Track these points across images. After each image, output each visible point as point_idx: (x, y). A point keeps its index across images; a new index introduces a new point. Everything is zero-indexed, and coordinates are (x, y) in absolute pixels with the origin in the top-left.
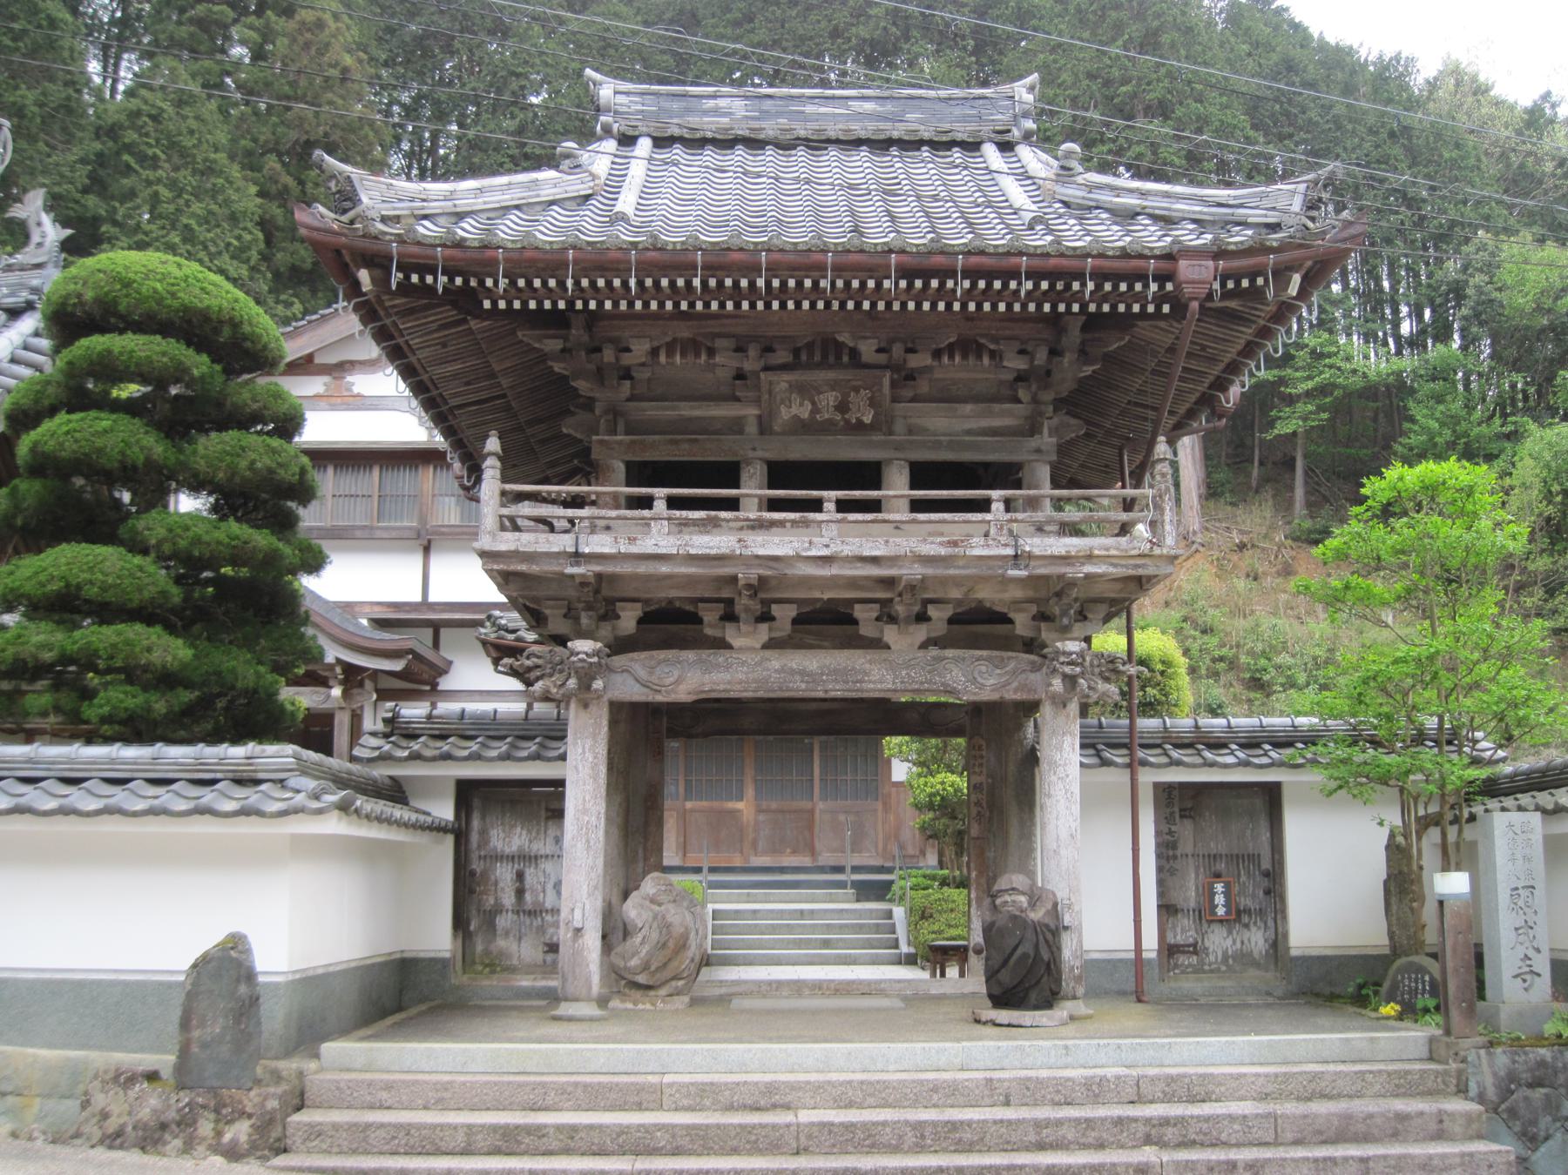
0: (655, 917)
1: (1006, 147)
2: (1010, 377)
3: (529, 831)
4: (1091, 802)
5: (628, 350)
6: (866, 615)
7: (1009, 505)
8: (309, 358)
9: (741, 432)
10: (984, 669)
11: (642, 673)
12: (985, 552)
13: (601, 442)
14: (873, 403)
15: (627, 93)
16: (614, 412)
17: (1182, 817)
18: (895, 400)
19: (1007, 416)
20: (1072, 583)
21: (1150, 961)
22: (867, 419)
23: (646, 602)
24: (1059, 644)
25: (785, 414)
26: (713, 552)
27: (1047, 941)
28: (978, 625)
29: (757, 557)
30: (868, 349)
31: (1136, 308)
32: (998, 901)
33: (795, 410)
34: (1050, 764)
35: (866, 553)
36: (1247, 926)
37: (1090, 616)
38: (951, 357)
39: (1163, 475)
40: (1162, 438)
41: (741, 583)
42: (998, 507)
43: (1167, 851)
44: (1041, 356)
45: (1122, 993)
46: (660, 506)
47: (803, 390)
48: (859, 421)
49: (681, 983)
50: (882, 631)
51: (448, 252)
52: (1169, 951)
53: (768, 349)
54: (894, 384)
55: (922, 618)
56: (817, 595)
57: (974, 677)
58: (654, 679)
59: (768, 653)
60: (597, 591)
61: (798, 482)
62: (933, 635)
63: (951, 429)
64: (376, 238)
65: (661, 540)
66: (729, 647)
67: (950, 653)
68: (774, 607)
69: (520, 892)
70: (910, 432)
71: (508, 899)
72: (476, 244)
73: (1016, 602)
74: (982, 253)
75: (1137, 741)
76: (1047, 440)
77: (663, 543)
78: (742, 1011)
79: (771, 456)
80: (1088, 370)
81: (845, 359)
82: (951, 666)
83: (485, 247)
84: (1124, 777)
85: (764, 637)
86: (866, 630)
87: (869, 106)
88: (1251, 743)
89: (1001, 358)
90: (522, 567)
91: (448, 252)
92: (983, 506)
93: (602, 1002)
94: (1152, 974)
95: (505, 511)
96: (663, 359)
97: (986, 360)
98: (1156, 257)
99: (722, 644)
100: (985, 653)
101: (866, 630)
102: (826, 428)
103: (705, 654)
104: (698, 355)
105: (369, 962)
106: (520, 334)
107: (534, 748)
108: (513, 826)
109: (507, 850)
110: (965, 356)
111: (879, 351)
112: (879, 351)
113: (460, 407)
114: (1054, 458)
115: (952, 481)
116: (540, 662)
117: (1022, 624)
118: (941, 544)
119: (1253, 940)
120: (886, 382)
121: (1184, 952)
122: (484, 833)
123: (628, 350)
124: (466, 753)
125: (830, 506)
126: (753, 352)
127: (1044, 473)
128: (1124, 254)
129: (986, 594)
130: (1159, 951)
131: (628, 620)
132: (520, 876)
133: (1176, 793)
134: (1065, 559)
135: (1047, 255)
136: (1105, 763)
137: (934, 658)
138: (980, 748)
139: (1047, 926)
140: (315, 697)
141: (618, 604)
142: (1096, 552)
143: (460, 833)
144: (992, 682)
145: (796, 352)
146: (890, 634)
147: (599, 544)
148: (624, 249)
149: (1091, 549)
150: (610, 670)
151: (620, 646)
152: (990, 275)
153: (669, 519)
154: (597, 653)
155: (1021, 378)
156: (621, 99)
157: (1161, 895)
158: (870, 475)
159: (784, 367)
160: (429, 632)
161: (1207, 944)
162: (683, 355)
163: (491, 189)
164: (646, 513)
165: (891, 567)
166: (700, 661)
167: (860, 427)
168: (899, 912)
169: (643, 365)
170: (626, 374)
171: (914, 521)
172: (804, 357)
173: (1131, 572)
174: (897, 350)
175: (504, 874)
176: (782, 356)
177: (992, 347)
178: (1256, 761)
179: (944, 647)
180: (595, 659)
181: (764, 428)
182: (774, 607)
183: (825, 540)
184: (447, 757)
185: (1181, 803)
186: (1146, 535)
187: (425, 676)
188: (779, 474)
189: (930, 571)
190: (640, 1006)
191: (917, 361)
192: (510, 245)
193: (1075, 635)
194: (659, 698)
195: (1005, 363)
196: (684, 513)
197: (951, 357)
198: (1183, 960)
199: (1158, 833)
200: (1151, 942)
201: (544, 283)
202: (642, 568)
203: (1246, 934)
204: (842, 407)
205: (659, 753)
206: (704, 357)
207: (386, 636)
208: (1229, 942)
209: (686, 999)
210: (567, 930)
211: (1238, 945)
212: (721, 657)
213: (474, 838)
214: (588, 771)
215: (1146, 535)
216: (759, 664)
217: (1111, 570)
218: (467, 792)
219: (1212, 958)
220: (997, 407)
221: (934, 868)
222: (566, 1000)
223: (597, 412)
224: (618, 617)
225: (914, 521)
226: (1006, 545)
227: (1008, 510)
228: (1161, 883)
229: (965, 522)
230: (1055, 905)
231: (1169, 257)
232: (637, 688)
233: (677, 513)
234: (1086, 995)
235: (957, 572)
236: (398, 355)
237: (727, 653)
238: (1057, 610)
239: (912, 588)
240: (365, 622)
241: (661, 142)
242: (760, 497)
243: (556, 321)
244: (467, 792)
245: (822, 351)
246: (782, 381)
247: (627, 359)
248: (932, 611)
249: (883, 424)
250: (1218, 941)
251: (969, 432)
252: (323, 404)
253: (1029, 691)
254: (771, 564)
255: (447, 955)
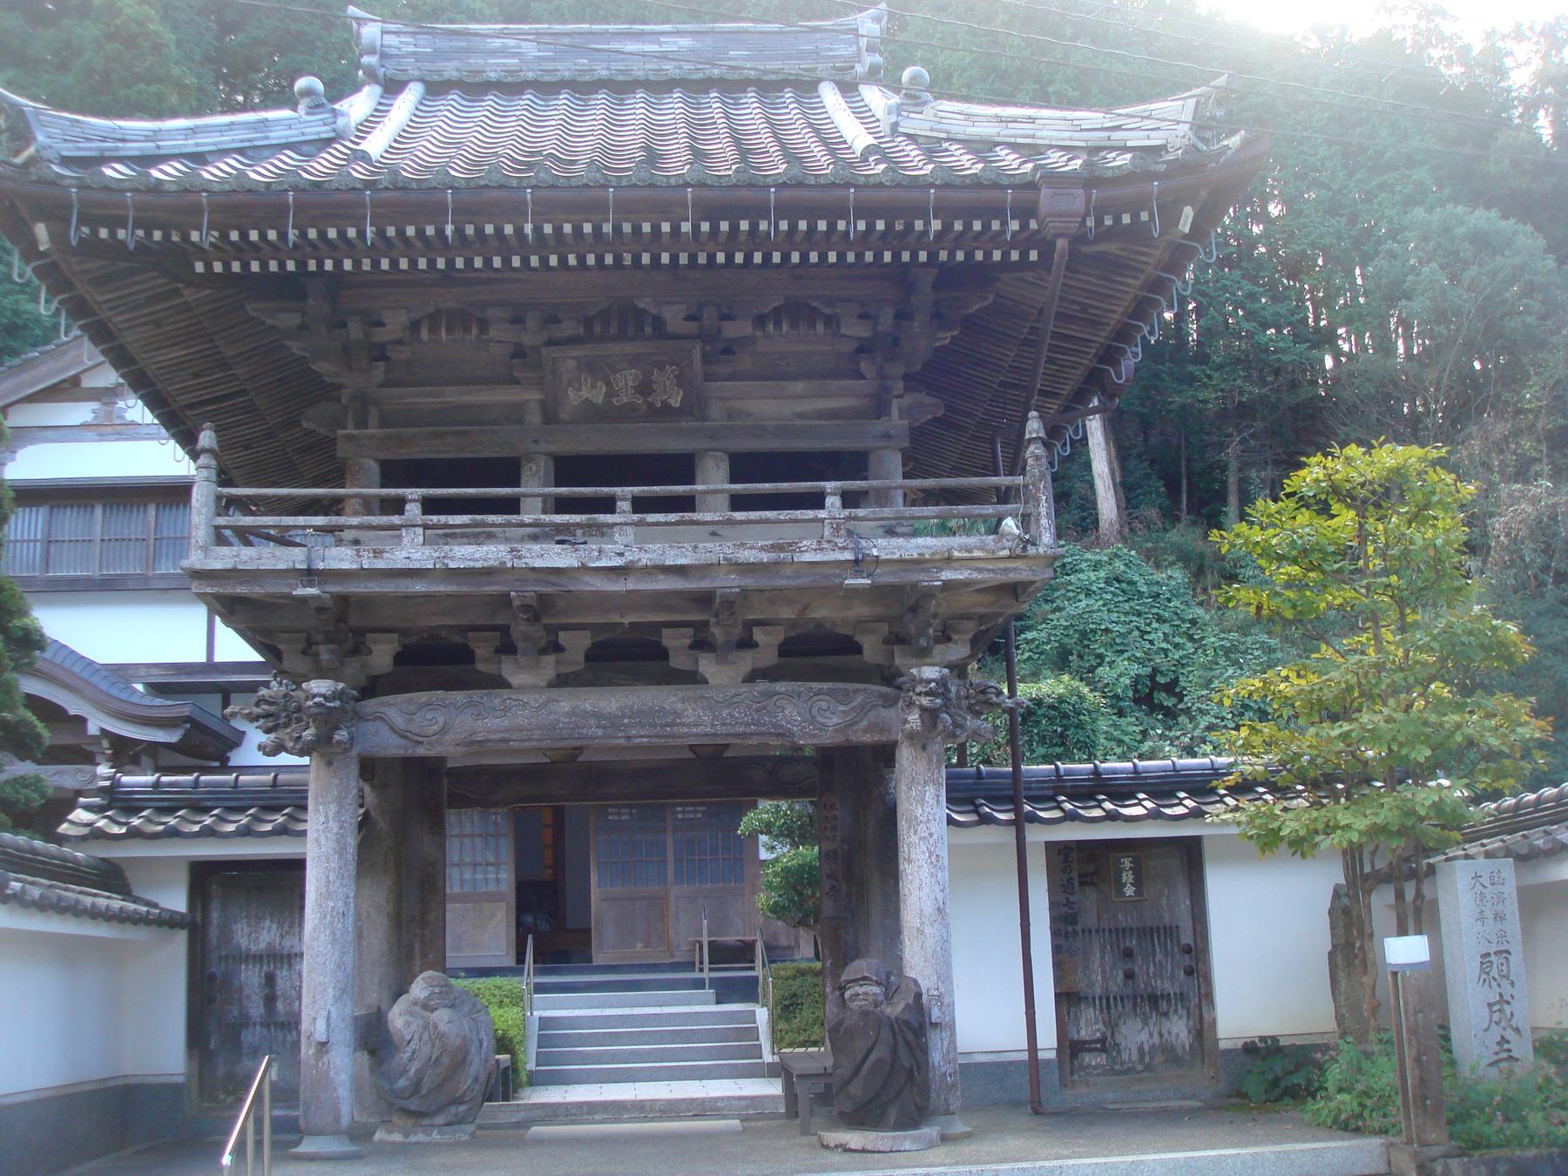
0: (426, 1027)
1: (848, 88)
2: (847, 347)
3: (281, 925)
4: (963, 867)
5: (382, 324)
6: (676, 643)
7: (850, 499)
8: (75, 381)
9: (520, 422)
10: (824, 705)
11: (399, 720)
12: (818, 557)
13: (350, 438)
14: (681, 381)
15: (397, 33)
16: (363, 402)
17: (1081, 884)
18: (708, 377)
19: (844, 396)
20: (929, 594)
21: (1048, 1062)
22: (675, 402)
23: (403, 632)
24: (914, 671)
25: (574, 398)
26: (478, 565)
27: (907, 1043)
28: (817, 652)
29: (534, 569)
30: (674, 317)
31: (997, 256)
32: (848, 994)
33: (585, 394)
34: (909, 821)
35: (669, 562)
36: (1166, 1014)
37: (955, 637)
38: (778, 325)
39: (1037, 458)
40: (1033, 414)
41: (516, 603)
42: (833, 501)
43: (1064, 925)
44: (887, 318)
45: (1015, 1104)
46: (413, 510)
47: (590, 367)
48: (666, 405)
49: (462, 1108)
50: (696, 662)
51: (138, 197)
52: (1070, 1047)
53: (554, 320)
54: (707, 359)
55: (747, 643)
56: (616, 618)
57: (813, 716)
58: (414, 727)
59: (555, 693)
60: (342, 619)
61: (588, 479)
62: (760, 665)
63: (779, 409)
64: (53, 183)
65: (414, 549)
66: (505, 685)
67: (781, 686)
68: (562, 634)
69: (270, 1000)
70: (730, 416)
71: (256, 1009)
72: (174, 188)
73: (860, 623)
74: (800, 185)
75: (1024, 793)
76: (896, 421)
77: (418, 556)
78: (539, 1141)
79: (555, 448)
80: (945, 338)
81: (648, 330)
82: (784, 703)
83: (186, 191)
84: (1009, 836)
85: (550, 673)
86: (678, 661)
87: (685, 42)
88: (1163, 788)
89: (838, 326)
90: (242, 590)
91: (138, 197)
92: (817, 501)
93: (360, 1134)
94: (1051, 1078)
95: (222, 521)
96: (424, 335)
97: (820, 328)
98: (1014, 187)
99: (499, 683)
100: (826, 686)
101: (678, 661)
102: (627, 414)
103: (476, 694)
104: (467, 330)
105: (72, 1090)
106: (248, 307)
107: (281, 819)
108: (261, 919)
109: (254, 948)
110: (794, 325)
111: (690, 318)
112: (689, 318)
113: (191, 406)
114: (906, 444)
115: (780, 474)
116: (272, 709)
117: (872, 649)
118: (762, 549)
119: (1175, 1030)
120: (697, 356)
121: (1090, 1050)
122: (226, 930)
123: (382, 324)
124: (196, 828)
125: (624, 505)
126: (532, 321)
127: (895, 462)
128: (976, 183)
129: (822, 612)
130: (1058, 1050)
131: (382, 655)
132: (270, 979)
133: (1074, 855)
134: (918, 563)
135: (880, 185)
136: (986, 820)
137: (762, 694)
138: (832, 806)
139: (907, 1023)
140: (79, 777)
141: (368, 636)
142: (956, 554)
143: (195, 926)
144: (835, 720)
145: (588, 323)
146: (707, 665)
147: (340, 558)
148: (355, 189)
149: (949, 551)
150: (359, 717)
151: (372, 687)
152: (812, 213)
153: (426, 527)
154: (336, 695)
155: (863, 348)
156: (391, 40)
157: (1058, 980)
158: (682, 467)
159: (573, 341)
160: (218, 698)
161: (1119, 1039)
162: (449, 330)
163: (207, 130)
164: (396, 519)
165: (701, 578)
166: (471, 704)
167: (666, 412)
168: (762, 1015)
169: (400, 342)
170: (379, 354)
171: (731, 522)
172: (597, 329)
173: (1002, 578)
174: (709, 314)
175: (251, 977)
176: (569, 328)
177: (827, 311)
178: (1168, 811)
179: (776, 680)
180: (337, 704)
181: (550, 416)
182: (562, 634)
183: (620, 548)
184: (173, 833)
185: (1080, 868)
186: (1017, 532)
187: (211, 750)
188: (568, 469)
189: (749, 582)
190: (413, 1138)
191: (732, 330)
192: (216, 187)
193: (937, 659)
194: (421, 751)
195: (843, 331)
196: (443, 519)
197: (778, 325)
198: (1088, 1059)
199: (1053, 905)
200: (1047, 1038)
201: (263, 236)
202: (389, 587)
203: (1166, 1025)
204: (644, 388)
205: (437, 824)
206: (475, 331)
207: (158, 701)
208: (1144, 1036)
209: (471, 1128)
210: (309, 1044)
211: (1156, 1039)
212: (497, 698)
213: (214, 933)
214: (332, 844)
215: (1017, 532)
216: (545, 704)
217: (975, 575)
218: (204, 876)
219: (1125, 1056)
220: (834, 384)
221: (809, 960)
222: (311, 1134)
223: (343, 401)
224: (370, 652)
225: (731, 522)
226: (844, 548)
227: (845, 506)
228: (1058, 966)
229: (792, 521)
230: (919, 996)
231: (1030, 185)
232: (394, 740)
233: (435, 518)
234: (965, 1108)
235: (784, 582)
236: (101, 334)
237: (505, 693)
238: (912, 629)
239: (729, 604)
240: (140, 687)
241: (435, 89)
242: (545, 497)
243: (289, 288)
244: (204, 876)
245: (625, 320)
246: (568, 360)
247: (379, 336)
248: (758, 635)
249: (694, 407)
250: (1135, 1035)
251: (802, 415)
252: (90, 434)
253: (882, 730)
254: (553, 579)
255: (181, 1080)
